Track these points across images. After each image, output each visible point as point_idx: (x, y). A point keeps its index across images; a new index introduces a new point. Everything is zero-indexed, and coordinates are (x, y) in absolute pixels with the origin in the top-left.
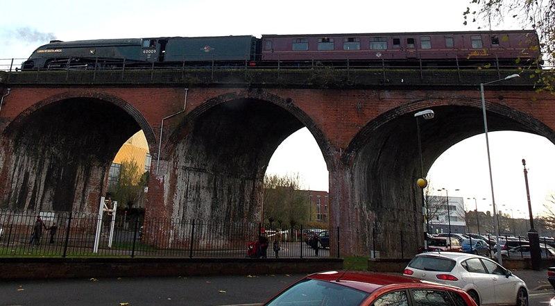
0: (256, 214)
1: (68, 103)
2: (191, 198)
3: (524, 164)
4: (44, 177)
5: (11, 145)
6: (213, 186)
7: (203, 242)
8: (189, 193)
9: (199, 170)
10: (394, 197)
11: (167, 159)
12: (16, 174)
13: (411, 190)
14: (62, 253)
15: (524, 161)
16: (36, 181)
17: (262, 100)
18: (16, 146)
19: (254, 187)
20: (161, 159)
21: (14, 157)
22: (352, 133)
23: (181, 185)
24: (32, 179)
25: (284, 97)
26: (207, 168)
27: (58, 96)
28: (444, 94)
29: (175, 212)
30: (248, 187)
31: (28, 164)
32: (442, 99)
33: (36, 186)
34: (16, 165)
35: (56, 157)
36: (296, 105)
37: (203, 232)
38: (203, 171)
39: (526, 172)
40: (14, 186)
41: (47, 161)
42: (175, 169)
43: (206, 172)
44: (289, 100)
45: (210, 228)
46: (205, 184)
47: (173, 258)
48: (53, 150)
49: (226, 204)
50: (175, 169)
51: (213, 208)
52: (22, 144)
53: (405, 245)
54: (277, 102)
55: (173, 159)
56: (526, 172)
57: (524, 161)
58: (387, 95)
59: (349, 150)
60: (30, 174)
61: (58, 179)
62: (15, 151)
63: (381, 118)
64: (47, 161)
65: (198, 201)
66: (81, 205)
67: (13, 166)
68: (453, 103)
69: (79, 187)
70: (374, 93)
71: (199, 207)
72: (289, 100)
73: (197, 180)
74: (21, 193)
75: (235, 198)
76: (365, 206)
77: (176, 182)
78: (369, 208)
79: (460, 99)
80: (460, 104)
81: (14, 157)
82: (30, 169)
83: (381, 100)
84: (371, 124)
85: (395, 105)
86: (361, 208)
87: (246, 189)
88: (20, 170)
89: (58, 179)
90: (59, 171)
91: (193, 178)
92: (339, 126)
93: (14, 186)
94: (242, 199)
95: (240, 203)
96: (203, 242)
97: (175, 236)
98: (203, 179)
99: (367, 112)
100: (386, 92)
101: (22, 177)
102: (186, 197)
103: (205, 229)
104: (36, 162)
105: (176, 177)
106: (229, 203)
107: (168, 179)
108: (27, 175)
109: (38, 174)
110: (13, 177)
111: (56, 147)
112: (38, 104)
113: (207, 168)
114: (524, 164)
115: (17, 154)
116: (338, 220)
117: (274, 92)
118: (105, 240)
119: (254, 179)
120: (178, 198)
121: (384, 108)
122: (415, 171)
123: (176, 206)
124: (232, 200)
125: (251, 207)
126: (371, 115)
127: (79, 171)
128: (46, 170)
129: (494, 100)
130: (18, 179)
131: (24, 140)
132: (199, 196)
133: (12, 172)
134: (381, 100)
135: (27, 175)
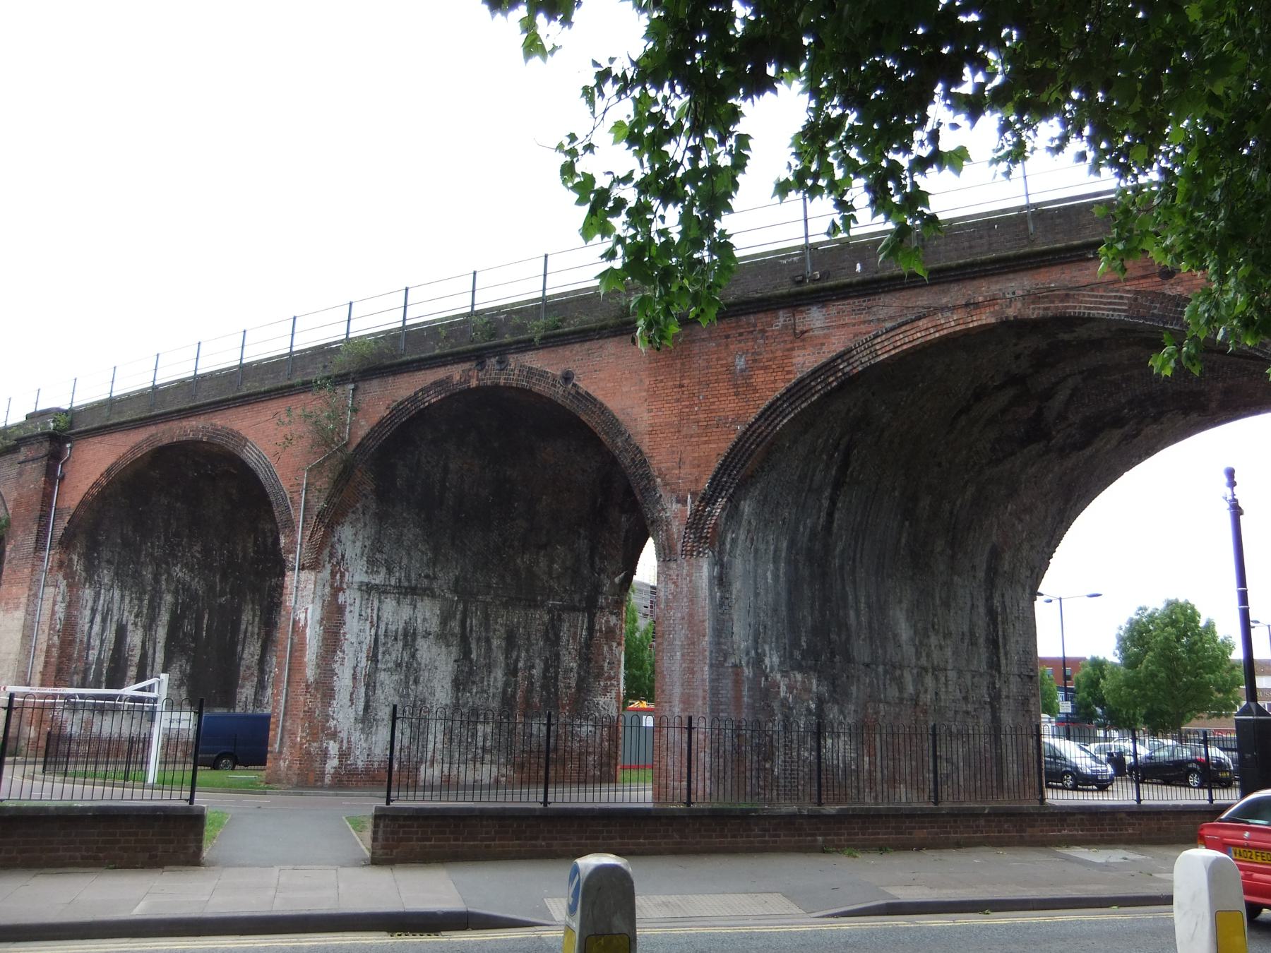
0: (601, 700)
1: (162, 456)
2: (386, 662)
3: (1232, 484)
4: (161, 633)
5: (78, 566)
6: (457, 630)
7: (429, 771)
8: (381, 650)
9: (408, 591)
10: (904, 631)
11: (315, 566)
12: (96, 628)
13: (982, 610)
14: (541, 798)
15: (1230, 473)
16: (143, 643)
17: (508, 388)
18: (91, 569)
19: (591, 629)
20: (302, 568)
21: (88, 593)
22: (718, 446)
23: (356, 630)
24: (135, 639)
25: (556, 370)
26: (435, 585)
27: (138, 446)
28: (984, 289)
29: (342, 696)
30: (573, 631)
31: (123, 606)
32: (977, 305)
33: (144, 656)
34: (94, 611)
35: (187, 589)
36: (584, 386)
37: (431, 746)
38: (429, 593)
39: (1236, 511)
40: (93, 656)
41: (168, 598)
42: (336, 590)
43: (433, 596)
44: (567, 377)
45: (449, 733)
46: (434, 625)
47: (1171, 803)
48: (178, 571)
49: (499, 674)
50: (336, 590)
51: (459, 684)
52: (103, 564)
53: (944, 768)
54: (540, 388)
55: (328, 567)
56: (1236, 511)
57: (1230, 473)
58: (815, 318)
59: (708, 499)
60: (130, 627)
61: (196, 638)
62: (89, 579)
63: (798, 390)
64: (168, 598)
65: (410, 671)
66: (256, 694)
67: (87, 613)
68: (1011, 313)
69: (250, 653)
70: (782, 319)
71: (416, 682)
72: (567, 377)
73: (405, 617)
74: (110, 670)
75: (529, 658)
76: (772, 660)
77: (341, 623)
78: (791, 664)
79: (1033, 297)
80: (1033, 312)
81: (88, 593)
82: (129, 618)
83: (800, 336)
84: (772, 410)
85: (837, 344)
86: (758, 661)
87: (564, 636)
88: (104, 620)
89: (196, 638)
90: (199, 619)
91: (394, 613)
92: (685, 431)
93: (93, 656)
94: (552, 662)
95: (546, 670)
96: (429, 771)
97: (343, 755)
98: (427, 613)
99: (760, 378)
100: (814, 309)
101: (111, 635)
102: (373, 658)
103: (435, 735)
104: (141, 600)
105: (340, 610)
106: (512, 671)
107: (318, 616)
108: (121, 632)
109: (149, 628)
110: (89, 637)
111: (186, 565)
112: (108, 471)
113: (435, 585)
114: (1232, 484)
115: (97, 587)
116: (676, 700)
117: (534, 360)
118: (170, 767)
119: (591, 608)
120: (349, 664)
121: (805, 360)
122: (995, 554)
123: (343, 681)
124: (521, 665)
125: (581, 680)
126: (771, 386)
127: (246, 617)
128: (165, 617)
129: (1145, 285)
130: (102, 642)
131: (106, 555)
132: (413, 656)
133: (87, 627)
134: (800, 336)
135: (121, 632)
